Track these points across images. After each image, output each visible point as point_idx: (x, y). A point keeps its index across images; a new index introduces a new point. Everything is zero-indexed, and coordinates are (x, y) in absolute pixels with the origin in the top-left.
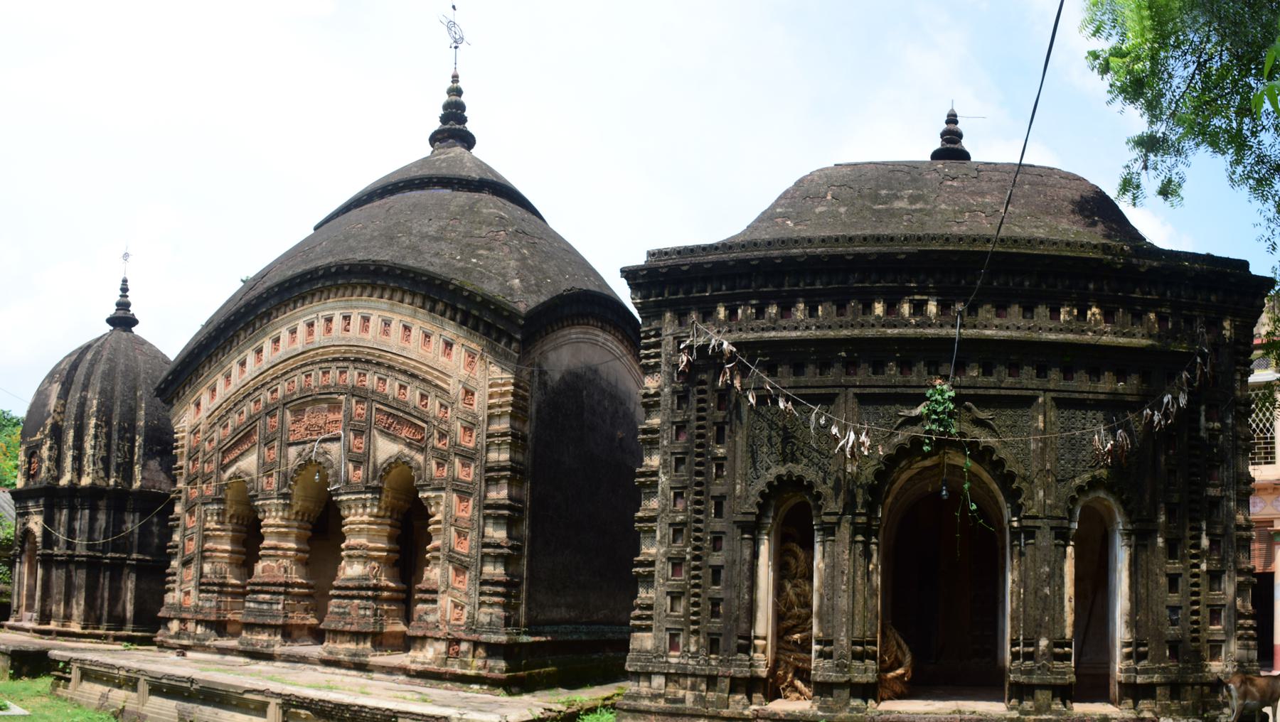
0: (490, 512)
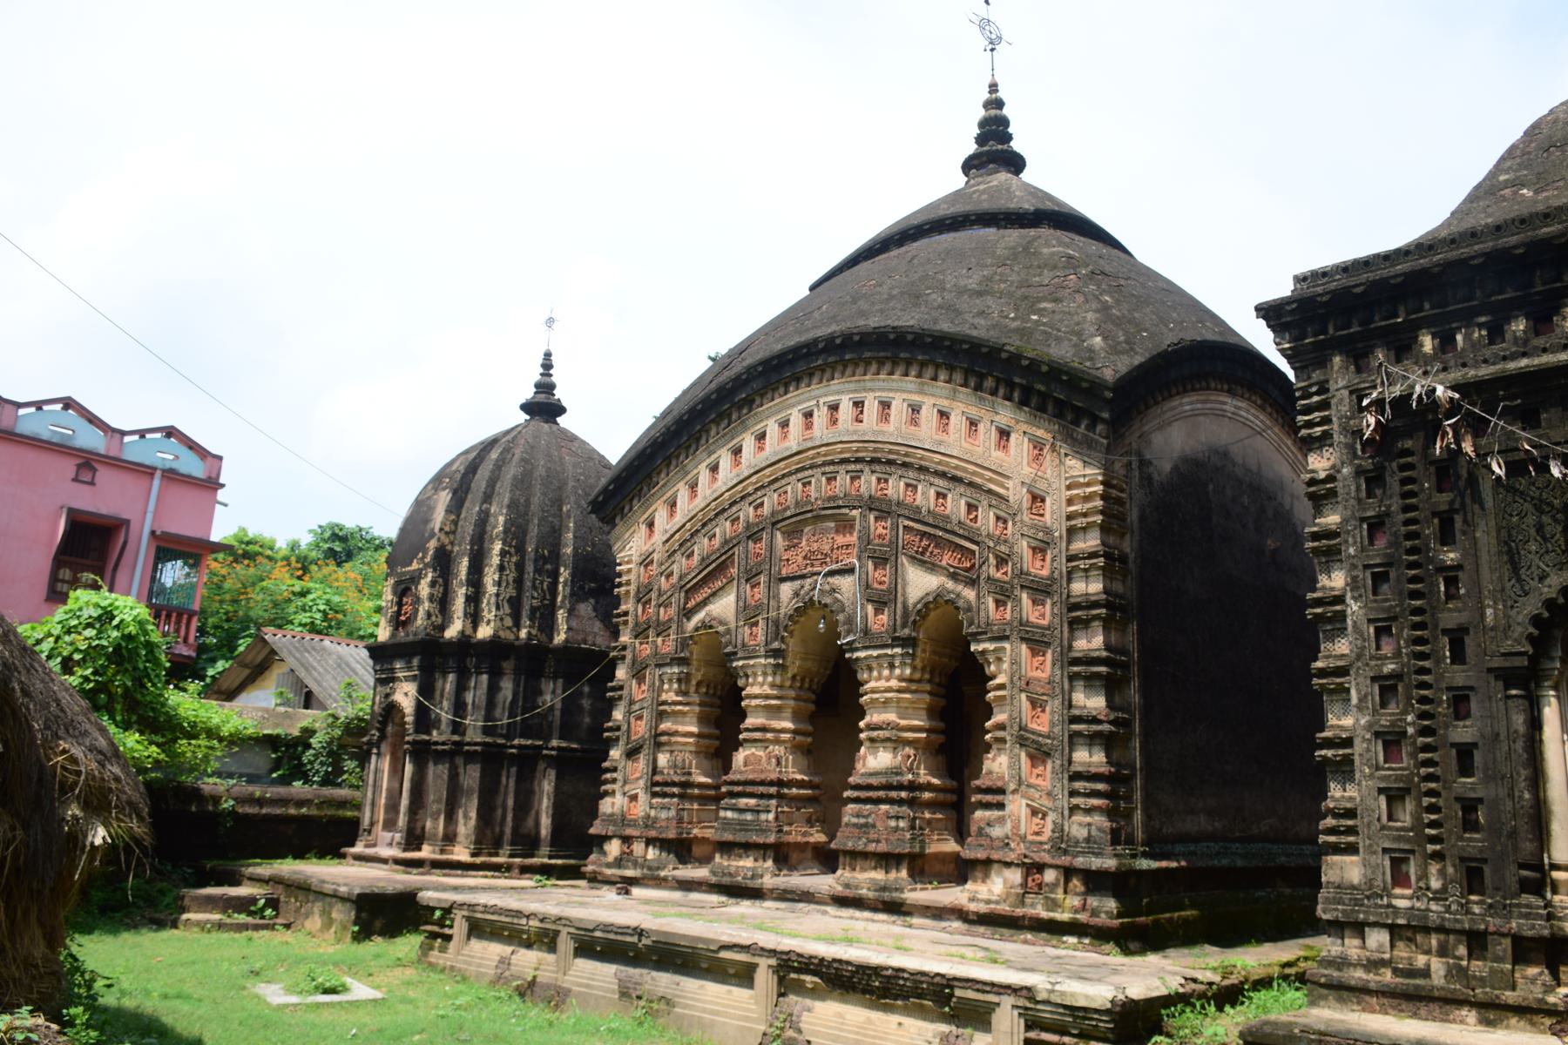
0: (1078, 669)
